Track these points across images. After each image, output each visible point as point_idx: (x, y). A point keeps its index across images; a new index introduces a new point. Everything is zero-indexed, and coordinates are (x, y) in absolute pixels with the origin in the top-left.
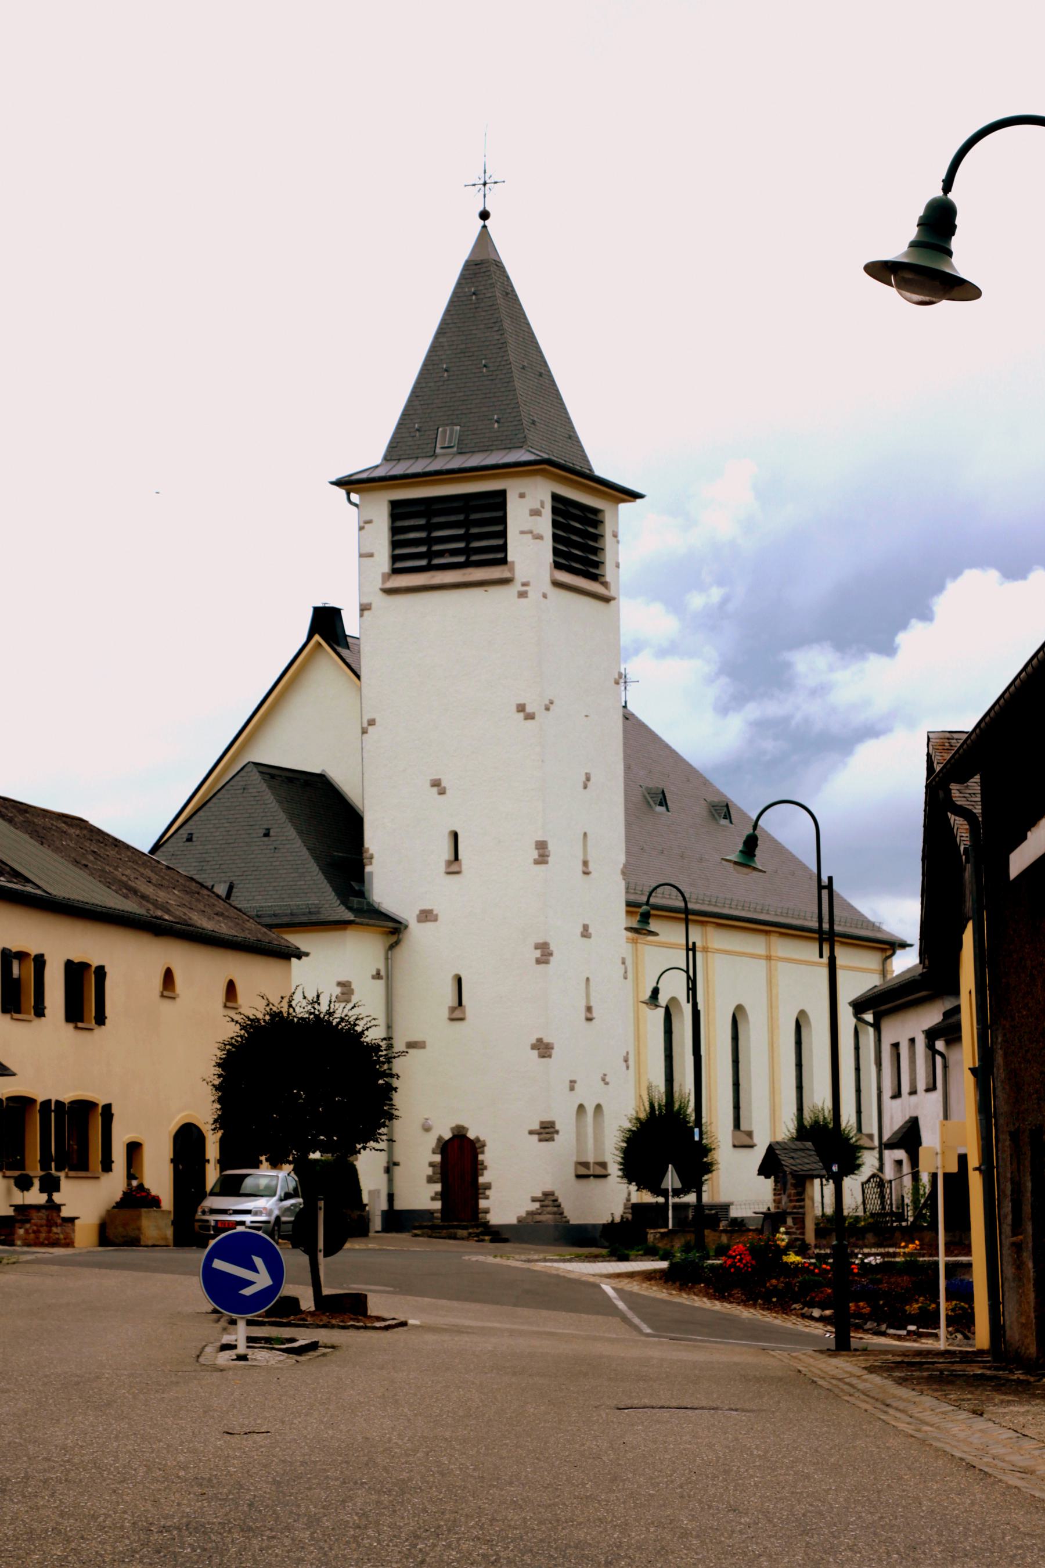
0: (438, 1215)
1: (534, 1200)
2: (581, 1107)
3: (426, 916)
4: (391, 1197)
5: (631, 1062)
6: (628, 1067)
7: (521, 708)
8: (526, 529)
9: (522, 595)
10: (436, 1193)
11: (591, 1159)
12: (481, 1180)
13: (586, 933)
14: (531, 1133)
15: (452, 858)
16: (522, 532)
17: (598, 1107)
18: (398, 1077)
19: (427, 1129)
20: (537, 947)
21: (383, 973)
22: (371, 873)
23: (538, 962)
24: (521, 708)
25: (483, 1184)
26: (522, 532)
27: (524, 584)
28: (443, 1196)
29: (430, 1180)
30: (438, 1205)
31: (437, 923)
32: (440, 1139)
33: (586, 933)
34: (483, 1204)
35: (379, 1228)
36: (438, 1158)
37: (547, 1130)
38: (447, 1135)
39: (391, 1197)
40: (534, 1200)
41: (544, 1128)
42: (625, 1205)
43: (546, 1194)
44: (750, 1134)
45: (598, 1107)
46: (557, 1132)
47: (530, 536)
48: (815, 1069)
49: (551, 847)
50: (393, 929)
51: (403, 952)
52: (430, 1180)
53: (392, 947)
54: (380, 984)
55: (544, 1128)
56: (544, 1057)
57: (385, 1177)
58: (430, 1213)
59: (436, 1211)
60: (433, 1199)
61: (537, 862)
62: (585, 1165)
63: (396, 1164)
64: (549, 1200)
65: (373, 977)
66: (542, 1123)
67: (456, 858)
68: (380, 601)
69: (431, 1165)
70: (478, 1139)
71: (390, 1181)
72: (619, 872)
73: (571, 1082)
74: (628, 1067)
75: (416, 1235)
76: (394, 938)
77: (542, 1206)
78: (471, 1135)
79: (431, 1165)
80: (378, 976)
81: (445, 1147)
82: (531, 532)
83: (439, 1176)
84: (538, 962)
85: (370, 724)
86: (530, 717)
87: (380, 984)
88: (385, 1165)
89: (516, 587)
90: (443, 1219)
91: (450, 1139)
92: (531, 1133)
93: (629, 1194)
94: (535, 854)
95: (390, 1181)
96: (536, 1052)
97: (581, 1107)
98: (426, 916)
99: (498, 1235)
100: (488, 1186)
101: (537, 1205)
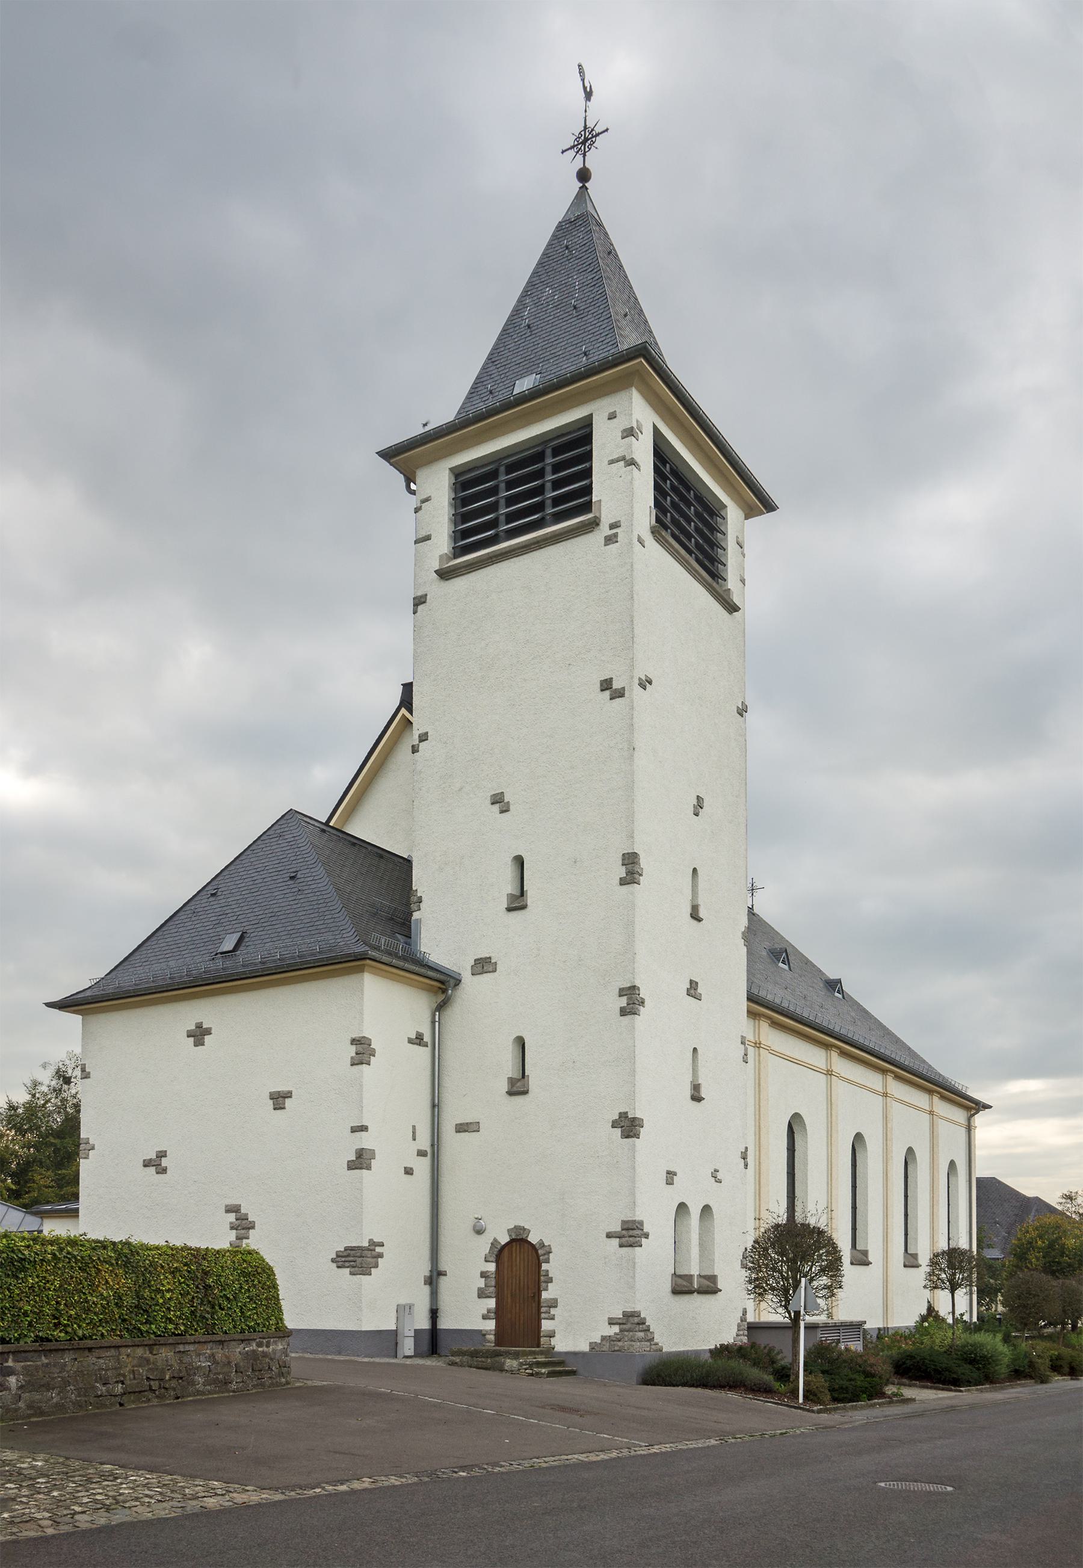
0: (492, 1337)
1: (612, 1322)
2: (682, 1208)
3: (484, 965)
4: (434, 1314)
5: (750, 1159)
6: (746, 1166)
7: (606, 685)
8: (615, 456)
9: (610, 540)
10: (489, 1311)
11: (695, 1271)
12: (545, 1295)
13: (693, 990)
14: (609, 1236)
15: (518, 894)
16: (611, 462)
17: (706, 1210)
18: (865, 1322)
19: (479, 1231)
20: (622, 992)
21: (427, 1038)
22: (419, 921)
23: (624, 1012)
24: (606, 685)
25: (547, 1300)
26: (611, 462)
27: (613, 526)
28: (499, 1314)
29: (482, 1294)
30: (491, 1325)
31: (495, 974)
32: (495, 1242)
33: (693, 990)
34: (546, 1325)
35: (411, 1353)
36: (491, 1267)
37: (631, 1233)
38: (504, 1239)
39: (434, 1314)
40: (612, 1322)
41: (627, 1229)
42: (739, 1325)
43: (628, 1315)
44: (865, 1253)
45: (706, 1210)
46: (647, 1236)
47: (622, 463)
48: (682, 1348)
49: (643, 862)
50: (442, 985)
51: (455, 1014)
52: (482, 1294)
53: (441, 1007)
54: (424, 1053)
55: (627, 1229)
56: (628, 1137)
57: (426, 1289)
58: (482, 1334)
59: (487, 1333)
60: (485, 1317)
61: (623, 882)
62: (689, 1278)
63: (441, 1274)
64: (632, 1322)
65: (410, 1041)
66: (624, 1222)
67: (522, 893)
68: (437, 589)
69: (483, 1275)
70: (542, 1244)
71: (434, 1295)
72: (740, 935)
73: (668, 1173)
74: (746, 1166)
75: (453, 1364)
76: (441, 997)
77: (621, 1331)
78: (533, 1239)
79: (483, 1275)
80: (419, 1040)
81: (501, 1254)
82: (623, 458)
83: (492, 1289)
84: (624, 1012)
85: (421, 741)
86: (619, 694)
87: (424, 1053)
88: (428, 1274)
89: (604, 530)
90: (499, 1341)
91: (507, 1244)
92: (609, 1236)
93: (745, 1312)
94: (622, 872)
95: (434, 1295)
96: (618, 1131)
97: (682, 1208)
98: (484, 965)
99: (561, 1367)
100: (554, 1304)
101: (616, 1329)
